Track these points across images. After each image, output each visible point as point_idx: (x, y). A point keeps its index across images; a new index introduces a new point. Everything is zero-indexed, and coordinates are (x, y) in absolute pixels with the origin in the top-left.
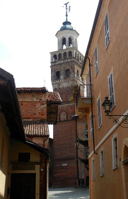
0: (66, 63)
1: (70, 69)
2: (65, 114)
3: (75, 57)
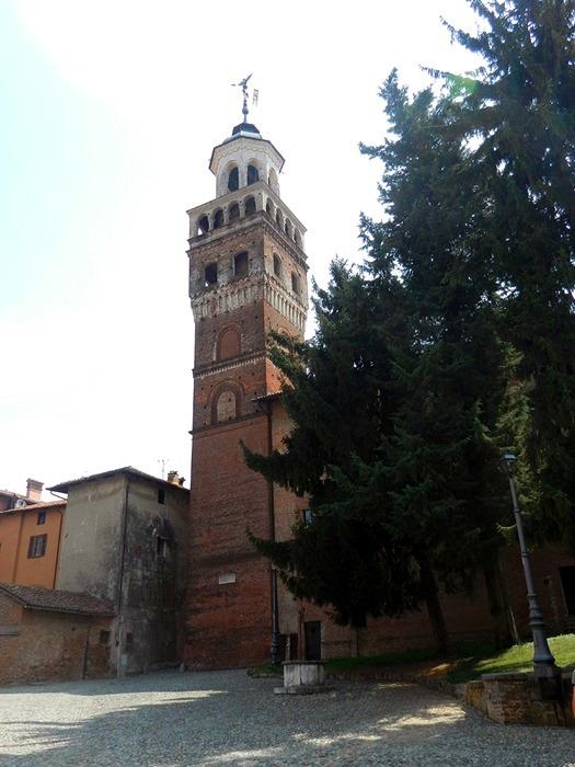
0: (236, 233)
1: (249, 250)
2: (234, 398)
3: (264, 209)
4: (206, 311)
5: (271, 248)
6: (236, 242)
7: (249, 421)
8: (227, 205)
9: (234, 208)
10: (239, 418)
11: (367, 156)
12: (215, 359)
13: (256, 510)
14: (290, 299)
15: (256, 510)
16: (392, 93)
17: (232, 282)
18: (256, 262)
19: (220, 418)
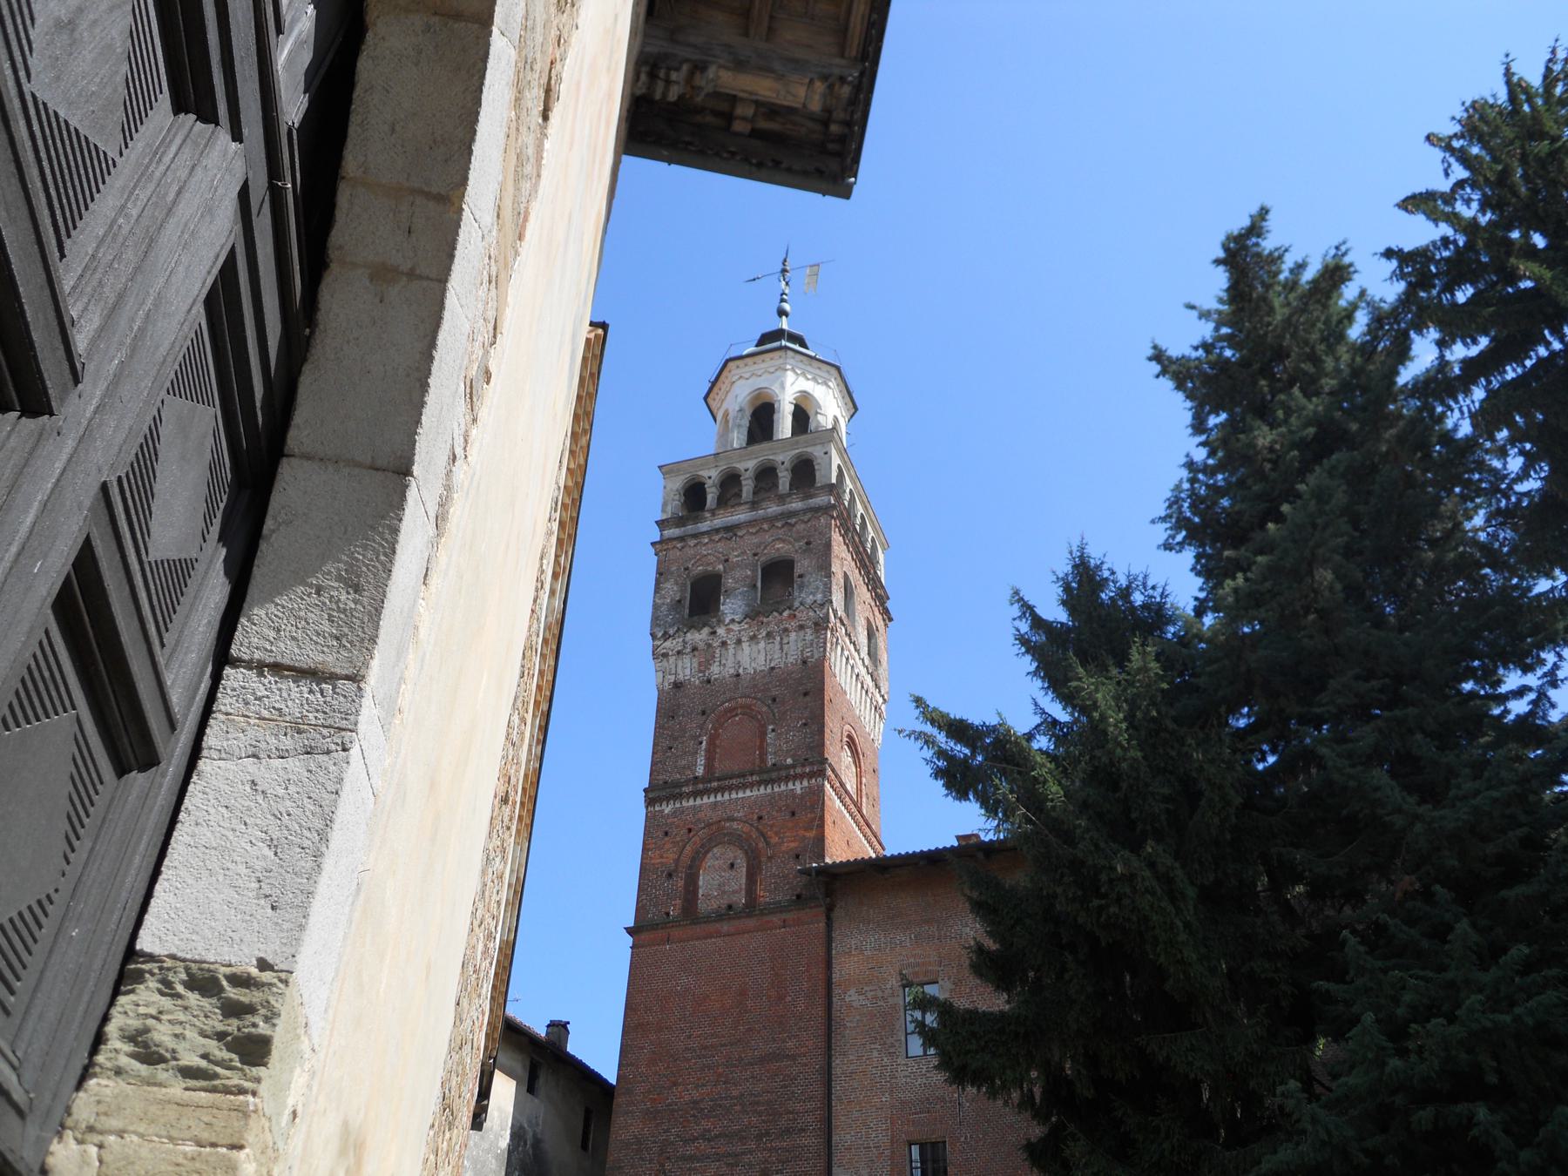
0: (771, 520)
1: (796, 557)
2: (742, 864)
4: (686, 669)
5: (842, 560)
6: (768, 538)
7: (776, 919)
8: (751, 464)
9: (766, 474)
10: (752, 907)
11: (1156, 368)
12: (700, 771)
13: (788, 1131)
14: (863, 671)
15: (788, 1131)
16: (1243, 257)
17: (753, 615)
18: (814, 580)
19: (703, 906)
